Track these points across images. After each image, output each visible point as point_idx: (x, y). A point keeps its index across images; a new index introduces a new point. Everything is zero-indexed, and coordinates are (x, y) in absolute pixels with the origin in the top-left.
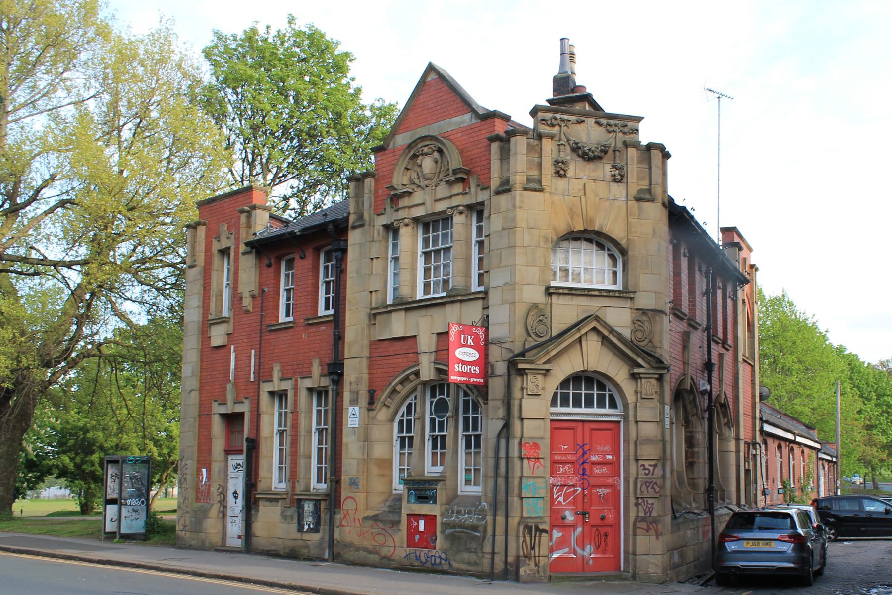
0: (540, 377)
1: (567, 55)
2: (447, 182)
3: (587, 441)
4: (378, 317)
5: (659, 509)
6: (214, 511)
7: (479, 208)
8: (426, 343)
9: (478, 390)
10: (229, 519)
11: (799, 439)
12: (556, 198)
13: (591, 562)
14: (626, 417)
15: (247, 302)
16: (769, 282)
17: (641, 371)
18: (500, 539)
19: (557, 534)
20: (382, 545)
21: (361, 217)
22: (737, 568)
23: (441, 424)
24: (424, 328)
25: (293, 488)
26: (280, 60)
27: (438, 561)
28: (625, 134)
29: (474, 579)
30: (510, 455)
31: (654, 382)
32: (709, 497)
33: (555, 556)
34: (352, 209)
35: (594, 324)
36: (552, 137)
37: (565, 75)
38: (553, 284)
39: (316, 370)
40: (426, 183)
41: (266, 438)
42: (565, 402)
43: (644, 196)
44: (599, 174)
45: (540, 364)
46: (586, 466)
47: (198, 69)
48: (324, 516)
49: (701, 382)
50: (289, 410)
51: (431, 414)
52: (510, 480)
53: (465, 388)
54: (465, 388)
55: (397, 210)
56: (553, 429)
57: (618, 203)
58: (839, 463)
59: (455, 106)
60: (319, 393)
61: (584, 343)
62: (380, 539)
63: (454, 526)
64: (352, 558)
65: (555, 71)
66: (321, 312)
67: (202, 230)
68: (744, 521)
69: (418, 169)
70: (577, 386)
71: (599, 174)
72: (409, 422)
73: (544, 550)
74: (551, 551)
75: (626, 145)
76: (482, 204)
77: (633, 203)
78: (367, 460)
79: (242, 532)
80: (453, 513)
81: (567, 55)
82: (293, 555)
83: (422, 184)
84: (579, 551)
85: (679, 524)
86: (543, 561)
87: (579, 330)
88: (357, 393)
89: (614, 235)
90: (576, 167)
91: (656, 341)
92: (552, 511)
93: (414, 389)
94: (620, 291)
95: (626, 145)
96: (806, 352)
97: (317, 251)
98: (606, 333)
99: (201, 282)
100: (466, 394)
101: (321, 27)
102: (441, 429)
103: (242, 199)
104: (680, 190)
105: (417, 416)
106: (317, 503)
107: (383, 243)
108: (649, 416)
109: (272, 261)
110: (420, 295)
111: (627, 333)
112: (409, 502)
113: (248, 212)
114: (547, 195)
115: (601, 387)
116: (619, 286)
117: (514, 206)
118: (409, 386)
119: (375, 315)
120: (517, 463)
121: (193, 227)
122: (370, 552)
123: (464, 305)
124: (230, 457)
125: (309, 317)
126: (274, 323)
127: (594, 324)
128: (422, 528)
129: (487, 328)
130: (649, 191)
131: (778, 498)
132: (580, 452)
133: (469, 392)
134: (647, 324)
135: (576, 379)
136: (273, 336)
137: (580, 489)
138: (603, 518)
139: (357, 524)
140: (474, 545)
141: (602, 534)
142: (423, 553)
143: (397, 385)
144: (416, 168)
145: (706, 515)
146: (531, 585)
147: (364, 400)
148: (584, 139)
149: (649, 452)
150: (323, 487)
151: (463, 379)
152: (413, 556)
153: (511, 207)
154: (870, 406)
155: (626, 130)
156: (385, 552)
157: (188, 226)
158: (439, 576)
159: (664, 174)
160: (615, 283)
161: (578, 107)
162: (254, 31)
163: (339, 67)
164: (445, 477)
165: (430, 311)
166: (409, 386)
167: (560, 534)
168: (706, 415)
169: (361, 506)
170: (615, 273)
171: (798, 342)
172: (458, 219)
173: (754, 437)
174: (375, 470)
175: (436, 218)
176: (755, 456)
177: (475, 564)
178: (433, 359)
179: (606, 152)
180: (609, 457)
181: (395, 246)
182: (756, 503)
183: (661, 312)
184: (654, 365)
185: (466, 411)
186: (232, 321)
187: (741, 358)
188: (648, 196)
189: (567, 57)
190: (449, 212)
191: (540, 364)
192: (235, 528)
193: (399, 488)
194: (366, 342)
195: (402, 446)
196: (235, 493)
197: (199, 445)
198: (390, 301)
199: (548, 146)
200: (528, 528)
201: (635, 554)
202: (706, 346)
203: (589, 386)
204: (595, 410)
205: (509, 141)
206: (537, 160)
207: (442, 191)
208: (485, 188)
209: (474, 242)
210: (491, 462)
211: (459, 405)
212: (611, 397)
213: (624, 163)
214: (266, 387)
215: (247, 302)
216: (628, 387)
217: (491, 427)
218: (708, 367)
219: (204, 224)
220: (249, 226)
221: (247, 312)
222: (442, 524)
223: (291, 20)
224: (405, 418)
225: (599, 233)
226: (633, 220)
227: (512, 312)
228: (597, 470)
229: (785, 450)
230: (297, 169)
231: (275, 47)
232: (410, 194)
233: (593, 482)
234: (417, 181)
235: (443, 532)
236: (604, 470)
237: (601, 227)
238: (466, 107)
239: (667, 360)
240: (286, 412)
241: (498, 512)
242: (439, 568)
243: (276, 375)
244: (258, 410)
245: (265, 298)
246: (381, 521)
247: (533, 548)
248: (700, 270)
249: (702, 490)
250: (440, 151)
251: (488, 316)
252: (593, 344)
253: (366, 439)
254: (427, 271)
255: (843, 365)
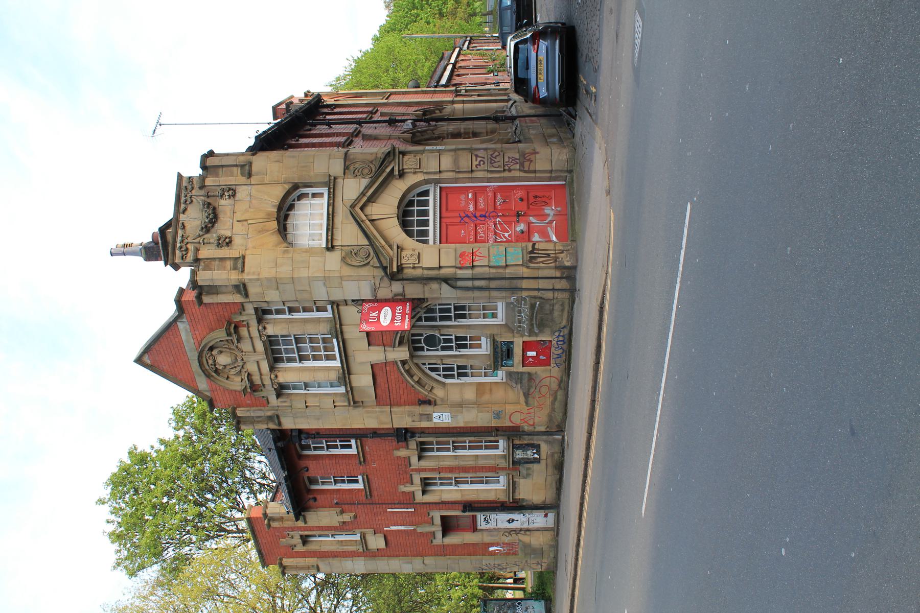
0: (404, 253)
1: (125, 250)
2: (238, 341)
3: (457, 214)
4: (357, 399)
5: (512, 152)
6: (525, 538)
7: (260, 312)
8: (377, 355)
9: (417, 307)
10: (531, 526)
11: (452, 61)
12: (250, 245)
13: (559, 209)
14: (437, 182)
15: (347, 517)
16: (321, 85)
17: (396, 169)
18: (542, 284)
19: (536, 237)
20: (549, 388)
21: (270, 418)
22: (561, 87)
23: (446, 341)
24: (365, 357)
25: (503, 469)
26: (137, 510)
27: (561, 338)
28: (193, 188)
29: (575, 306)
30: (470, 277)
31: (406, 158)
32: (502, 120)
33: (554, 239)
34: (264, 427)
35: (357, 209)
36: (197, 250)
37: (143, 251)
38: (324, 245)
39: (402, 453)
40: (239, 360)
41: (462, 495)
42: (425, 233)
43: (247, 170)
44: (228, 209)
45: (393, 253)
46: (478, 214)
47: (147, 582)
48: (526, 440)
49: (405, 127)
50: (438, 476)
51: (437, 350)
52: (491, 276)
53: (415, 319)
54: (415, 319)
55: (264, 385)
56: (447, 242)
57: (254, 193)
58: (471, 35)
59: (172, 337)
60: (422, 449)
61: (374, 217)
62: (544, 390)
63: (532, 325)
64: (561, 414)
65: (140, 259)
66: (353, 451)
67: (287, 562)
68: (521, 84)
69: (228, 368)
70: (411, 223)
71: (228, 209)
72: (445, 369)
73: (550, 246)
74: (551, 241)
75: (202, 187)
76: (256, 309)
77: (254, 180)
78: (478, 404)
79: (541, 513)
80: (520, 327)
81: (125, 250)
82: (560, 467)
83: (241, 364)
84: (550, 219)
85: (525, 139)
86: (559, 247)
87: (363, 221)
88: (421, 415)
89: (282, 195)
90: (223, 229)
91: (372, 158)
92: (517, 241)
93: (417, 365)
94: (329, 188)
95: (202, 187)
96: (378, 66)
97: (301, 457)
98: (365, 199)
99: (331, 559)
100: (420, 319)
101: (107, 476)
102: (450, 341)
103: (259, 529)
104: (238, 141)
105: (439, 362)
106: (516, 447)
107: (293, 397)
108: (437, 161)
109: (311, 496)
110: (337, 363)
111: (365, 182)
112: (512, 366)
113: (269, 520)
114: (248, 252)
115: (411, 203)
116: (325, 190)
117: (258, 280)
118: (415, 370)
119: (354, 402)
120: (477, 270)
121: (284, 569)
122: (555, 399)
123: (344, 322)
124: (479, 527)
125: (357, 461)
126: (364, 493)
127: (357, 209)
128: (534, 354)
129: (363, 301)
130: (242, 166)
131: (502, 76)
132: (466, 220)
133: (418, 316)
134: (357, 166)
135: (405, 224)
136: (375, 493)
137: (498, 219)
138: (522, 200)
139: (532, 411)
140: (547, 307)
141: (535, 200)
142: (555, 352)
143: (413, 380)
144: (226, 370)
145: (517, 122)
146: (580, 256)
147: (427, 409)
148: (199, 222)
149: (465, 162)
150: (502, 443)
151: (407, 319)
152: (558, 361)
153: (259, 283)
154: (422, 14)
155: (189, 187)
156: (554, 386)
157: (284, 574)
158: (574, 336)
159: (227, 155)
160: (321, 195)
161: (169, 238)
162: (111, 535)
163: (142, 459)
164: (490, 335)
165: (350, 353)
166: (415, 370)
167: (536, 234)
168: (433, 123)
169: (517, 408)
170: (314, 195)
171: (370, 72)
172: (270, 331)
173: (451, 92)
174: (486, 397)
175: (269, 352)
176: (466, 91)
177: (562, 305)
178: (391, 349)
179: (209, 204)
180: (470, 195)
181: (295, 388)
182: (506, 89)
183: (346, 154)
184: (392, 158)
185: (433, 319)
186: (363, 530)
187: (385, 101)
188: (247, 168)
189: (126, 249)
190: (264, 338)
191: (393, 253)
192: (538, 520)
193: (501, 375)
194: (378, 409)
195: (465, 375)
196: (509, 521)
197: (469, 555)
198: (342, 390)
199: (204, 253)
200: (532, 259)
201: (551, 171)
202: (375, 125)
203: (411, 213)
204: (431, 208)
205: (201, 286)
206: (217, 262)
207: (246, 346)
208: (242, 306)
209: (290, 317)
210: (477, 294)
211: (429, 325)
212: (419, 195)
213: (218, 188)
214: (419, 497)
215: (347, 517)
216: (411, 180)
217: (447, 295)
218: (392, 122)
219: (281, 559)
220: (281, 519)
221: (355, 517)
222: (530, 336)
223: (101, 502)
224: (442, 373)
225: (280, 208)
226: (268, 179)
227: (350, 278)
228: (482, 205)
229: (462, 71)
230: (232, 493)
231: (125, 515)
232: (249, 375)
233: (491, 209)
234: (239, 369)
235: (536, 335)
236: (481, 200)
237: (274, 206)
238: (172, 328)
239: (387, 149)
240: (440, 479)
241: (519, 286)
242: (567, 337)
243: (408, 489)
244: (439, 503)
245: (343, 502)
246: (529, 390)
247: (548, 255)
248: (310, 130)
249: (496, 126)
250: (211, 349)
251: (353, 301)
252: (375, 210)
253: (460, 405)
254: (315, 358)
255: (391, 38)
